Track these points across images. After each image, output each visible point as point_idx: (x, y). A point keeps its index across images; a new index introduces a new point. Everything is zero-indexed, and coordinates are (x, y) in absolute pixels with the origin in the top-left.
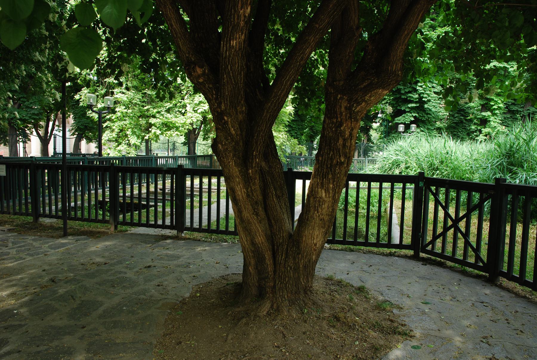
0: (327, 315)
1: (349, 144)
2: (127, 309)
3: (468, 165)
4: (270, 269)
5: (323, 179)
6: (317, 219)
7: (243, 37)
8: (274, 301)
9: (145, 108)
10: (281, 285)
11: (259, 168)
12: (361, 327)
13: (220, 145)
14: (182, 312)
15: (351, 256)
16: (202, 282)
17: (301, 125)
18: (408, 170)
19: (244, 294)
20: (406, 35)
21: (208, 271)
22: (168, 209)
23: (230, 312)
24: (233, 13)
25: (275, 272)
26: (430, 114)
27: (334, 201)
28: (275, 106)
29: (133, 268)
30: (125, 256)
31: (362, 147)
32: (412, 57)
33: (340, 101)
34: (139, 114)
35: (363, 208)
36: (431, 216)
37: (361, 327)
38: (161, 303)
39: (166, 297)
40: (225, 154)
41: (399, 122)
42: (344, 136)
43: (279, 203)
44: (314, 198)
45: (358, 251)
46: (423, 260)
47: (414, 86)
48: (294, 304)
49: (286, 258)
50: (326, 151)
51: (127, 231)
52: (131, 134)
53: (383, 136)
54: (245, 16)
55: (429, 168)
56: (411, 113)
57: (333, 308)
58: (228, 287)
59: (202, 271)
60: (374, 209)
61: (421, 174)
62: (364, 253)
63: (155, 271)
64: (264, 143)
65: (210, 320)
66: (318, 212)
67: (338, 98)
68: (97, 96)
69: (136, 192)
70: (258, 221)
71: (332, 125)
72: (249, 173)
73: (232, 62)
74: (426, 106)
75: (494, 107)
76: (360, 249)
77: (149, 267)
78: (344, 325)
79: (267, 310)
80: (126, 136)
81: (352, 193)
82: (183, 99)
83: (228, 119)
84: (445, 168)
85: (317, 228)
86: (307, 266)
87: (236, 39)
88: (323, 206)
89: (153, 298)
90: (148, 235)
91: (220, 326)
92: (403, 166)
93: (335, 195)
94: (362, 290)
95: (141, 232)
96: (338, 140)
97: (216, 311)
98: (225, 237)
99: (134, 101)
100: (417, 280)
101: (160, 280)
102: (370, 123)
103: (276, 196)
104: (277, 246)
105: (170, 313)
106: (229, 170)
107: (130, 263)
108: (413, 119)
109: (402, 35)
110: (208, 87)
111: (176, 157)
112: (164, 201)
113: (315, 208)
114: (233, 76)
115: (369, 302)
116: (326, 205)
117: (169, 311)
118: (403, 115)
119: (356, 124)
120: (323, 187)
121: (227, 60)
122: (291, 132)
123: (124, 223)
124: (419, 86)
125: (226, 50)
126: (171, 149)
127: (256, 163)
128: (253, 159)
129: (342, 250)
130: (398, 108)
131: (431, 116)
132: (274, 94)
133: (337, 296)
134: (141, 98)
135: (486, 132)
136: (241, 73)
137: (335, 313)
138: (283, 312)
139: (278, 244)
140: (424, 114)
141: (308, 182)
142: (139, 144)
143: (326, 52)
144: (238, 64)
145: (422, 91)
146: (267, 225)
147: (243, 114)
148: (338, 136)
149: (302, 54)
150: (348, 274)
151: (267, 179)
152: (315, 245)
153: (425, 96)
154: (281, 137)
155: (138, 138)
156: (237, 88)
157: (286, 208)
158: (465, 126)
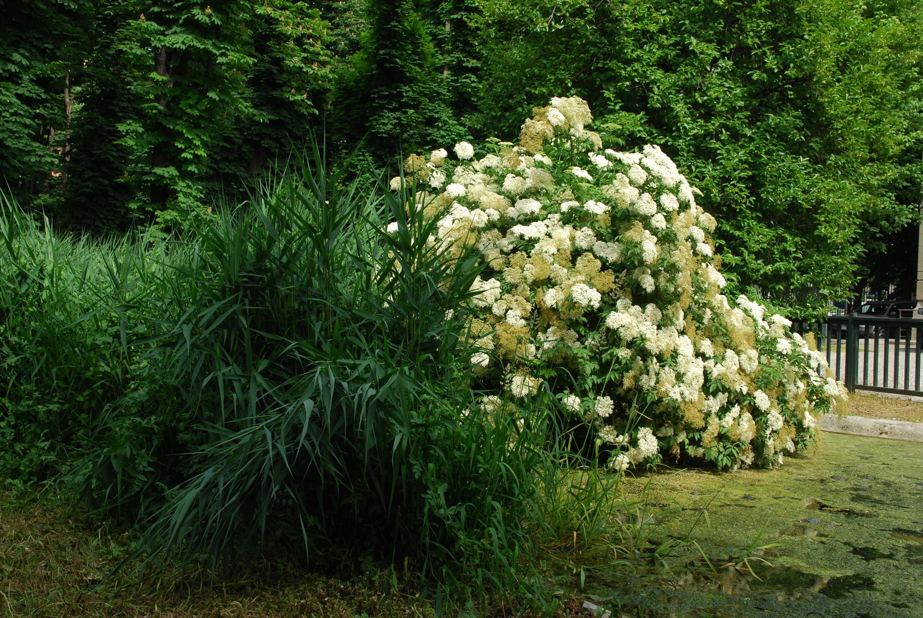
3: (104, 324)
75: (184, 155)
84: (14, 339)
135: (166, 221)
158: (114, 205)
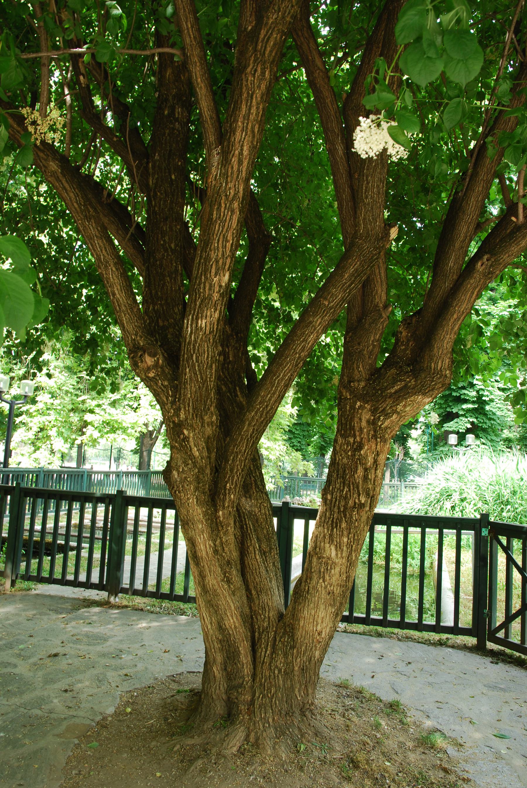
0: (337, 756)
1: (373, 476)
2: (5, 736)
4: (247, 670)
5: (332, 529)
6: (323, 592)
7: (217, 315)
8: (251, 728)
9: (80, 399)
10: (264, 700)
11: (235, 509)
12: (394, 781)
13: (175, 473)
14: (97, 744)
15: (378, 644)
16: (138, 686)
17: (308, 431)
18: (465, 503)
19: (203, 714)
20: (455, 320)
21: (149, 667)
22: (97, 555)
23: (178, 746)
24: (203, 281)
25: (254, 676)
26: (494, 420)
27: (350, 564)
28: (261, 417)
29: (29, 657)
30: (19, 634)
31: (397, 465)
32: (465, 346)
33: (360, 411)
34: (70, 407)
35: (398, 561)
36: (501, 576)
37: (394, 781)
38: (65, 724)
39: (75, 713)
40: (183, 486)
41: (450, 429)
42: (365, 464)
43: (264, 563)
44: (319, 558)
45: (390, 636)
46: (492, 654)
47: (470, 380)
48: (283, 733)
49: (272, 654)
50: (337, 485)
51: (30, 589)
52: (56, 434)
53: (426, 449)
54: (220, 286)
55: (496, 500)
56: (467, 417)
57: (348, 743)
58: (178, 697)
59: (140, 666)
60: (414, 563)
61: (485, 516)
62: (399, 640)
63: (63, 664)
64: (242, 471)
65: (142, 762)
66: (324, 581)
67: (357, 407)
68: (12, 378)
69: (50, 525)
70: (230, 592)
71: (347, 446)
72: (219, 517)
73: (198, 350)
74: (487, 408)
76: (393, 633)
77: (56, 655)
78: (365, 776)
79: (238, 744)
80: (48, 437)
81: (379, 547)
82: (137, 388)
83: (189, 433)
85: (322, 607)
86: (307, 669)
87: (206, 317)
88: (333, 571)
89: (53, 716)
90: (62, 598)
91: (158, 774)
92: (456, 497)
93: (350, 554)
94: (395, 707)
95: (52, 593)
96: (357, 470)
97: (154, 743)
98: (182, 605)
99: (64, 388)
100: (484, 692)
101: (68, 681)
102: (407, 430)
103: (260, 551)
104: (259, 633)
105: (77, 746)
106: (188, 511)
107: (25, 648)
108: (469, 426)
109: (450, 320)
110: (162, 384)
111: (120, 472)
112: (92, 540)
113: (320, 575)
114: (199, 370)
115: (406, 731)
116: (337, 569)
117: (76, 741)
118: (455, 420)
119: (384, 446)
120: (333, 541)
121: (192, 347)
122: (293, 441)
123: (27, 577)
124: (477, 379)
125: (191, 333)
126: (115, 458)
127: (230, 500)
128: (225, 495)
129: (364, 634)
130: (448, 409)
131: (495, 423)
132: (260, 399)
133: (355, 719)
134: (75, 384)
136: (211, 366)
137: (351, 752)
138: (264, 748)
139: (261, 630)
140: (484, 419)
141: (312, 523)
142: (66, 451)
143: (342, 335)
144: (208, 354)
145: (481, 387)
146: (244, 598)
147: (213, 426)
148: (356, 463)
149: (303, 341)
150: (373, 677)
151: (246, 525)
152: (319, 634)
153: (486, 393)
154: (278, 448)
155: (66, 441)
156: (204, 389)
157: (276, 572)
